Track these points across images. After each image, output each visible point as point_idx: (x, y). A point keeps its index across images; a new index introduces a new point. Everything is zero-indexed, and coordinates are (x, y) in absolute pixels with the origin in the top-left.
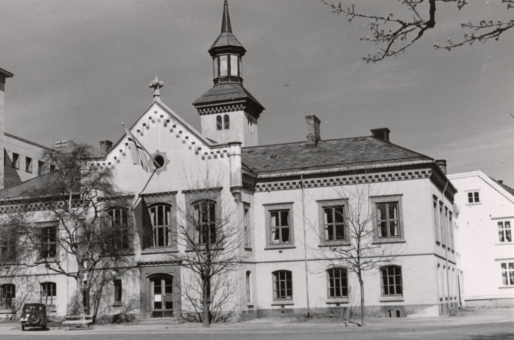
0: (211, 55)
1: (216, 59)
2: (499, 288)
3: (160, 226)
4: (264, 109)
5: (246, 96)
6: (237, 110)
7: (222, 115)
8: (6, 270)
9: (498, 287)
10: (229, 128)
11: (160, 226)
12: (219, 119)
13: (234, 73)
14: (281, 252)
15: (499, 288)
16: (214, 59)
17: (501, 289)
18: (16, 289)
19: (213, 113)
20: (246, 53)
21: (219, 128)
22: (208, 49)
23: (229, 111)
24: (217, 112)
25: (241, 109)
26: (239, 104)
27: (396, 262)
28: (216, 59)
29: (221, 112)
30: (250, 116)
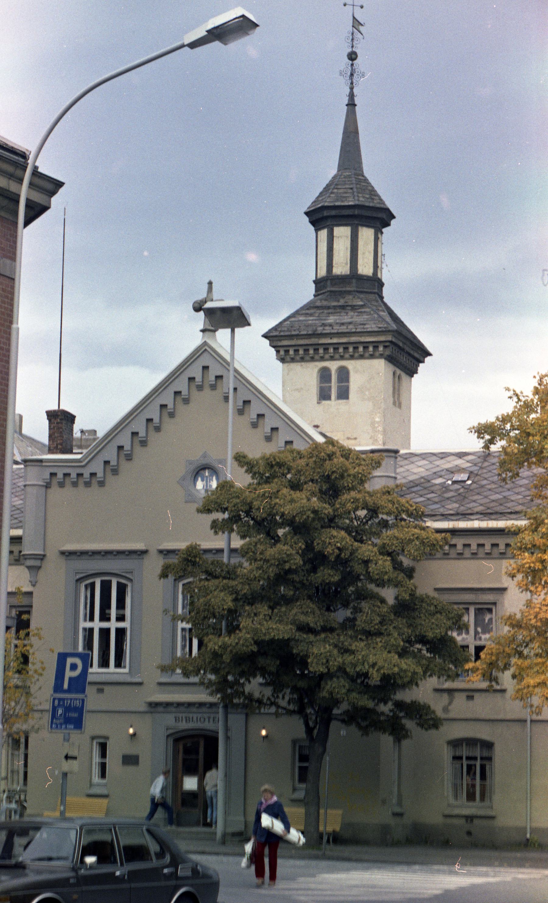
0: (313, 223)
1: (323, 234)
2: (210, 283)
3: (105, 625)
4: (429, 354)
5: (394, 326)
6: (372, 357)
7: (333, 366)
8: (457, 662)
9: (213, 280)
10: (347, 398)
11: (105, 625)
12: (325, 375)
13: (365, 268)
14: (101, 691)
15: (210, 283)
16: (317, 231)
17: (206, 286)
18: (177, 730)
19: (313, 359)
20: (393, 222)
21: (324, 395)
22: (305, 209)
23: (352, 357)
24: (322, 359)
25: (381, 356)
26: (376, 345)
27: (483, 733)
28: (323, 234)
29: (332, 358)
30: (398, 372)
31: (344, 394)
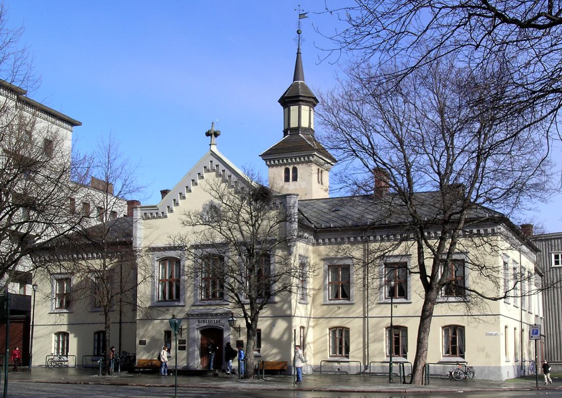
12: (287, 171)
21: (287, 179)
31: (295, 179)
